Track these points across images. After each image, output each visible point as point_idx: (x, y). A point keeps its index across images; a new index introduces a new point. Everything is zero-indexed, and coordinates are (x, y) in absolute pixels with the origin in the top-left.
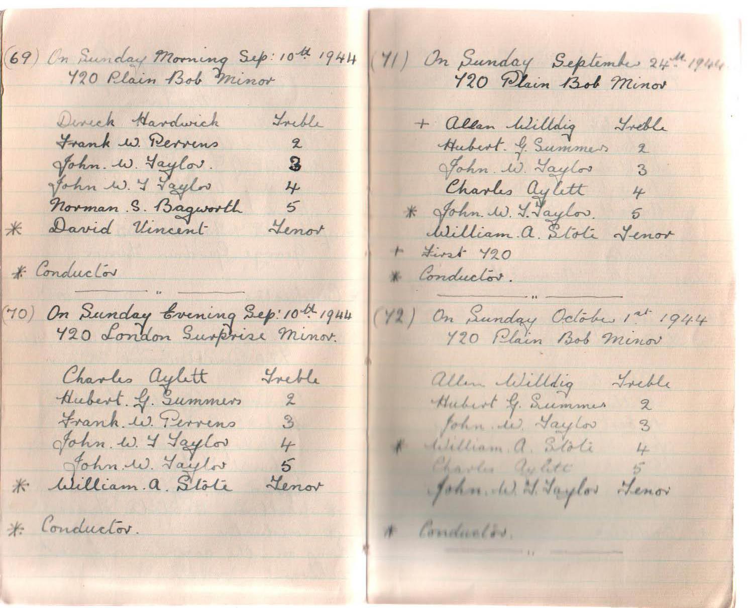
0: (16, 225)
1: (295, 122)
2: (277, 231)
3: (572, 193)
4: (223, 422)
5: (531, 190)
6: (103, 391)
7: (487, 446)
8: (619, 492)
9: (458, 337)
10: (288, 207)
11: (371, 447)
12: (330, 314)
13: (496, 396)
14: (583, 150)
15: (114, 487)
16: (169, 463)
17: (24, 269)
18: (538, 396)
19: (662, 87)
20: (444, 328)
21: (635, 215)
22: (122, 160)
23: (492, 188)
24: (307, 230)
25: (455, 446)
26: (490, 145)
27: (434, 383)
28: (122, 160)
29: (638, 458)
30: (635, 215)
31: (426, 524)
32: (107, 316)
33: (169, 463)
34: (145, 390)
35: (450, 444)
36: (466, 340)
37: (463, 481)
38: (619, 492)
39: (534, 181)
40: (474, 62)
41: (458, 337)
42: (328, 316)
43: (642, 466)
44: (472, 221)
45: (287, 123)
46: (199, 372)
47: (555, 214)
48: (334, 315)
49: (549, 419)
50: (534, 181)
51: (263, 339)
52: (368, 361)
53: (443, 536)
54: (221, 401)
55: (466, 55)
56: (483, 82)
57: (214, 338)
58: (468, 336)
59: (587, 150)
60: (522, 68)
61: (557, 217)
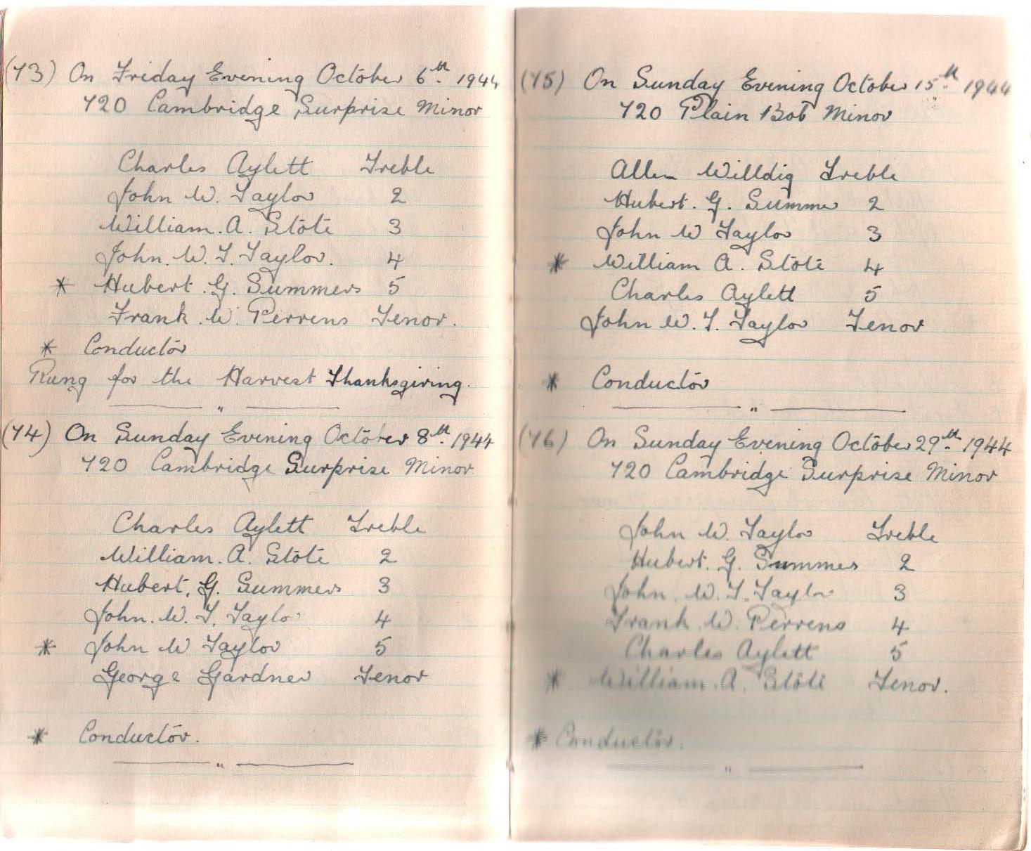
3: (785, 268)
7: (680, 680)
8: (869, 685)
11: (518, 525)
15: (192, 230)
17: (53, 644)
18: (248, 575)
21: (870, 296)
23: (676, 291)
25: (635, 681)
30: (896, 654)
34: (214, 575)
35: (627, 678)
36: (635, 473)
38: (869, 685)
44: (647, 246)
47: (773, 535)
49: (769, 583)
52: (512, 501)
54: (313, 590)
60: (712, 92)
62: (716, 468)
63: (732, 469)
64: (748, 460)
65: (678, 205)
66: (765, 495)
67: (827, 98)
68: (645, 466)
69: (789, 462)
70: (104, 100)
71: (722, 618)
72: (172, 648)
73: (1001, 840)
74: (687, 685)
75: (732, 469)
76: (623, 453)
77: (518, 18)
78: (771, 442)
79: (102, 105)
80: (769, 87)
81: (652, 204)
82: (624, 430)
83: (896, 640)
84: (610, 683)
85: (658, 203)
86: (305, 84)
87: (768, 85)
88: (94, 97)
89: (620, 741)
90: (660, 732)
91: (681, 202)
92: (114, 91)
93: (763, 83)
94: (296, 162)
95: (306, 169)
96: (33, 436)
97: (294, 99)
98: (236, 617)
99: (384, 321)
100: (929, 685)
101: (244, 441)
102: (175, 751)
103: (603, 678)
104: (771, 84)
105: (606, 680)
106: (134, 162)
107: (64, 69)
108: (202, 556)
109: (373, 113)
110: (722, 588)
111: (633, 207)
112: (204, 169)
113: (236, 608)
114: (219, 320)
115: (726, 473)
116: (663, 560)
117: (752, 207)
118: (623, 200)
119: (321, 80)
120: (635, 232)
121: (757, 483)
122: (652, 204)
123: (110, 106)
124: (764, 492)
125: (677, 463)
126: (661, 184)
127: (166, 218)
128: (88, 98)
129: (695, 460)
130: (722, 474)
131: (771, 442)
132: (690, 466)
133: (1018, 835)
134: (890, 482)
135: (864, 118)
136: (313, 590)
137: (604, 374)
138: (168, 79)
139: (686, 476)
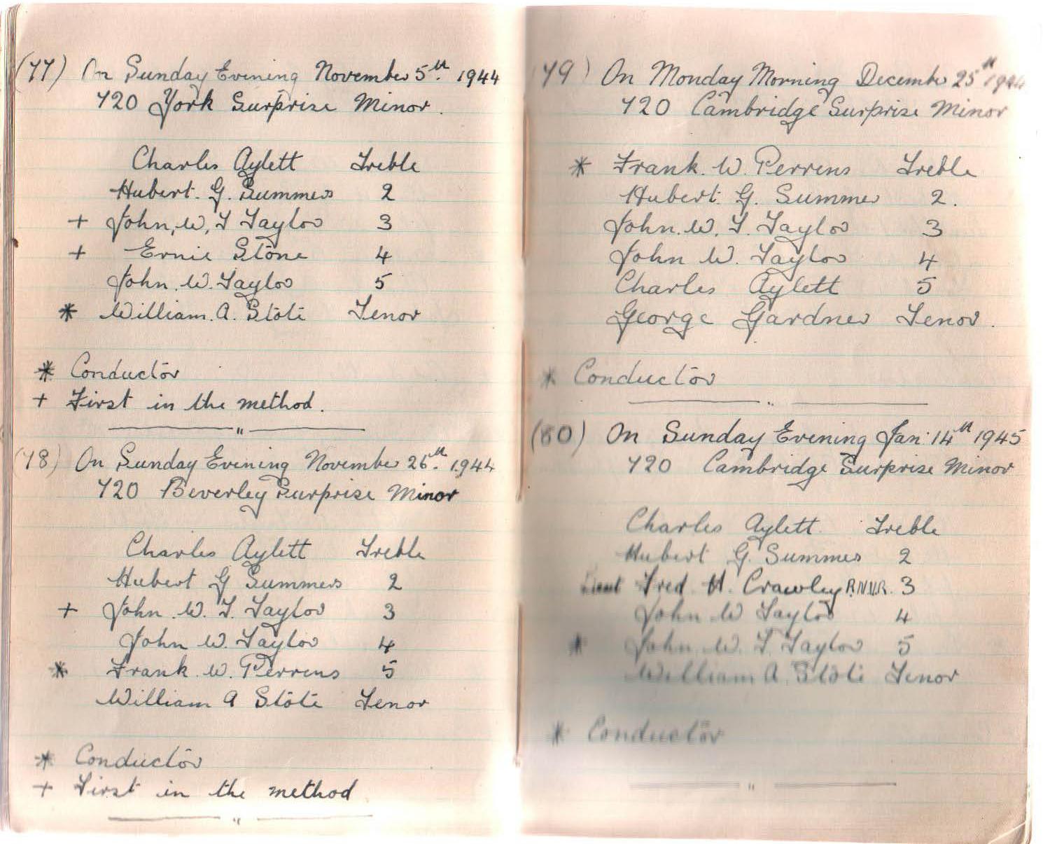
0: (66, 314)
1: (381, 164)
2: (910, 320)
9: (643, 464)
10: (376, 282)
20: (625, 450)
22: (187, 219)
24: (176, 313)
26: (269, 104)
27: (630, 527)
28: (187, 219)
29: (902, 630)
31: (597, 723)
32: (732, 471)
36: (654, 468)
40: (247, 107)
41: (643, 464)
43: (909, 641)
45: (267, 107)
48: (995, 438)
53: (622, 740)
54: (318, 585)
55: (157, 105)
56: (565, 434)
58: (657, 463)
62: (756, 463)
63: (774, 462)
64: (789, 454)
66: (803, 490)
69: (831, 456)
70: (117, 97)
71: (734, 610)
72: (726, 615)
73: (1008, 832)
74: (736, 679)
75: (774, 462)
78: (813, 436)
79: (115, 101)
82: (650, 424)
83: (386, 659)
84: (649, 675)
88: (108, 93)
89: (657, 734)
90: (707, 724)
91: (187, 191)
92: (127, 91)
93: (349, 72)
95: (296, 163)
97: (213, 93)
98: (256, 611)
99: (912, 322)
100: (946, 676)
103: (641, 673)
105: (645, 673)
107: (76, 66)
109: (302, 110)
110: (212, 608)
111: (134, 196)
112: (217, 166)
115: (764, 469)
120: (142, 222)
121: (796, 478)
123: (122, 104)
124: (803, 487)
125: (216, 464)
126: (163, 175)
129: (736, 455)
130: (761, 469)
131: (813, 436)
132: (730, 461)
133: (1024, 827)
134: (870, 475)
135: (400, 109)
137: (587, 367)
138: (185, 77)
139: (725, 470)
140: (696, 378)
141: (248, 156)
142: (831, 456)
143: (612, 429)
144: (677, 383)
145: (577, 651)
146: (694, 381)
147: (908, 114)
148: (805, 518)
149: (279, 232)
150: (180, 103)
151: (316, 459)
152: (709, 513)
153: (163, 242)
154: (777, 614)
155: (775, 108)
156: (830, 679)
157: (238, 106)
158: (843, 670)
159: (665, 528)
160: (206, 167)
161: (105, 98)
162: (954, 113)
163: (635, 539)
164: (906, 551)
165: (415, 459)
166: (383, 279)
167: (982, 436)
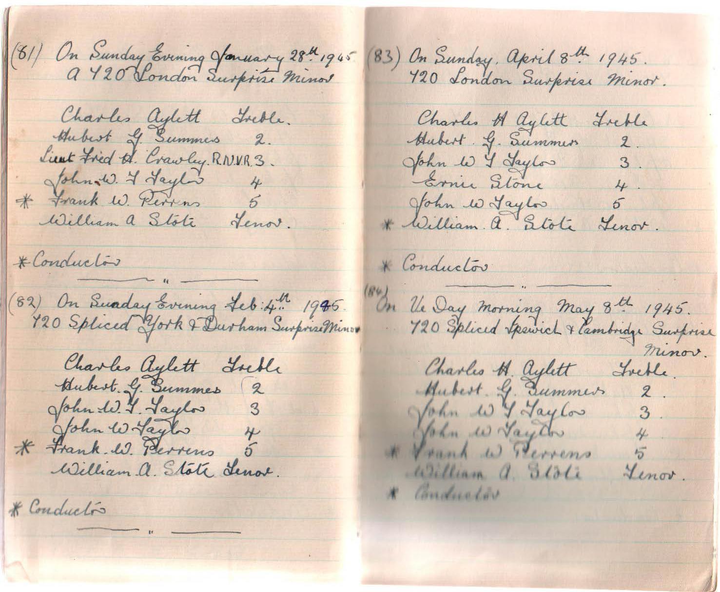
4: (580, 389)
5: (527, 371)
6: (104, 377)
12: (658, 307)
13: (111, 131)
14: (561, 394)
16: (154, 177)
19: (670, 478)
33: (154, 177)
37: (447, 425)
39: (435, 82)
42: (656, 309)
43: (644, 450)
44: (445, 213)
46: (560, 116)
50: (435, 82)
51: (645, 125)
54: (582, 392)
57: (235, 80)
58: (430, 326)
59: (561, 144)
61: (171, 185)
65: (105, 139)
67: (286, 66)
68: (56, 319)
76: (84, 312)
77: (371, 15)
80: (171, 58)
81: (441, 141)
85: (89, 137)
86: (33, 57)
87: (170, 56)
94: (193, 114)
96: (271, 309)
101: (171, 307)
102: (97, 519)
104: (173, 56)
106: (74, 113)
108: (188, 389)
113: (230, 362)
114: (418, 225)
115: (612, 330)
116: (450, 389)
117: (514, 143)
118: (421, 139)
119: (412, 60)
122: (441, 141)
127: (465, 158)
128: (413, 73)
136: (582, 392)
140: (476, 267)
141: (526, 117)
142: (600, 320)
143: (40, 298)
144: (465, 271)
145: (392, 456)
146: (474, 269)
147: (584, 83)
148: (570, 364)
149: (526, 168)
150: (466, 79)
151: (564, 305)
152: (475, 362)
153: (441, 174)
154: (516, 433)
155: (575, 79)
156: (554, 476)
157: (528, 80)
158: (563, 470)
159: (89, 367)
160: (468, 123)
161: (416, 75)
162: (622, 84)
163: (69, 375)
164: (258, 385)
165: (48, 319)
166: (620, 201)
167: (309, 306)
